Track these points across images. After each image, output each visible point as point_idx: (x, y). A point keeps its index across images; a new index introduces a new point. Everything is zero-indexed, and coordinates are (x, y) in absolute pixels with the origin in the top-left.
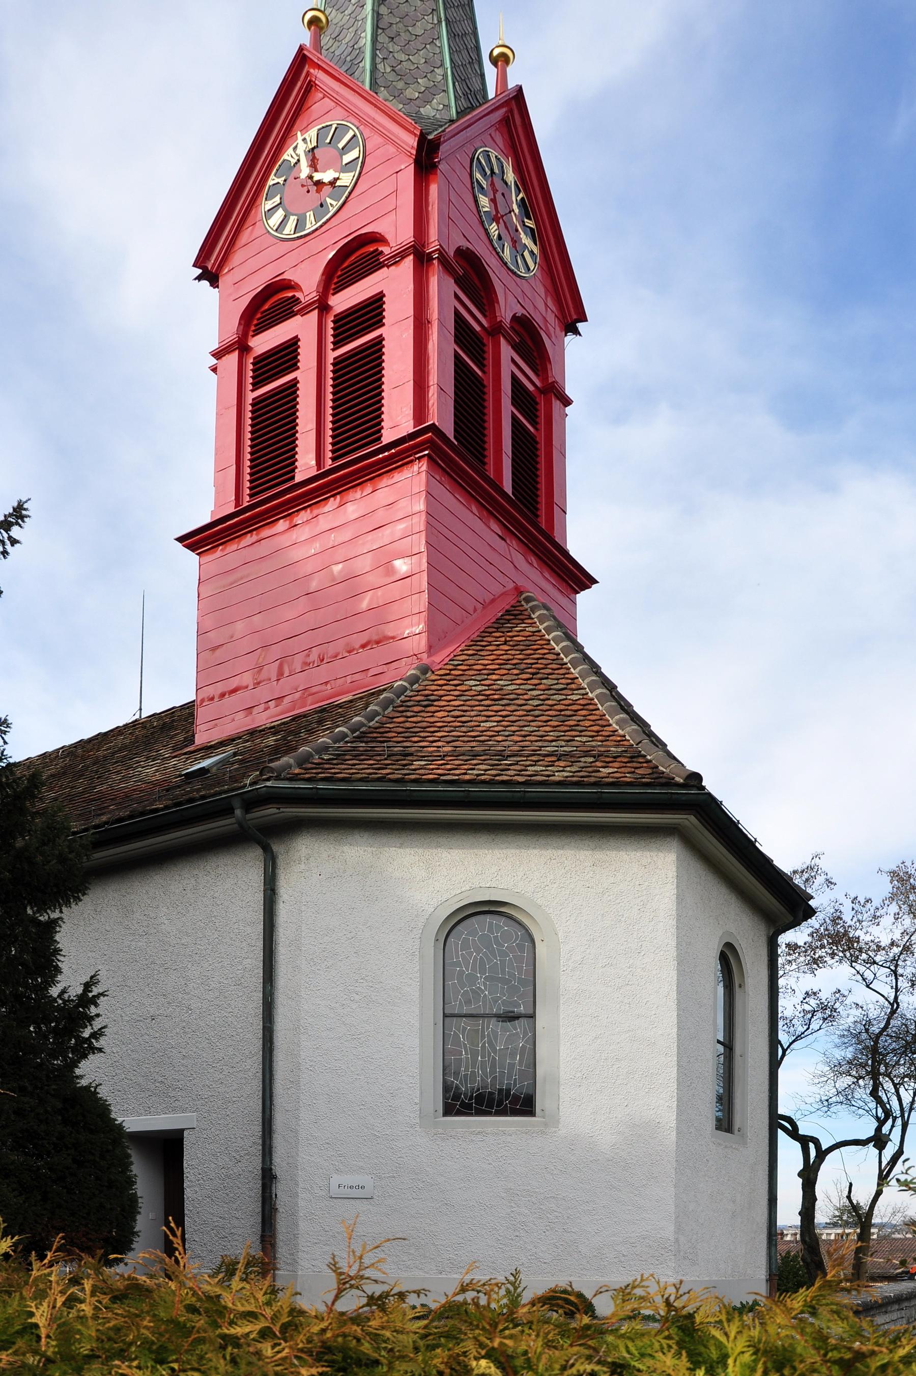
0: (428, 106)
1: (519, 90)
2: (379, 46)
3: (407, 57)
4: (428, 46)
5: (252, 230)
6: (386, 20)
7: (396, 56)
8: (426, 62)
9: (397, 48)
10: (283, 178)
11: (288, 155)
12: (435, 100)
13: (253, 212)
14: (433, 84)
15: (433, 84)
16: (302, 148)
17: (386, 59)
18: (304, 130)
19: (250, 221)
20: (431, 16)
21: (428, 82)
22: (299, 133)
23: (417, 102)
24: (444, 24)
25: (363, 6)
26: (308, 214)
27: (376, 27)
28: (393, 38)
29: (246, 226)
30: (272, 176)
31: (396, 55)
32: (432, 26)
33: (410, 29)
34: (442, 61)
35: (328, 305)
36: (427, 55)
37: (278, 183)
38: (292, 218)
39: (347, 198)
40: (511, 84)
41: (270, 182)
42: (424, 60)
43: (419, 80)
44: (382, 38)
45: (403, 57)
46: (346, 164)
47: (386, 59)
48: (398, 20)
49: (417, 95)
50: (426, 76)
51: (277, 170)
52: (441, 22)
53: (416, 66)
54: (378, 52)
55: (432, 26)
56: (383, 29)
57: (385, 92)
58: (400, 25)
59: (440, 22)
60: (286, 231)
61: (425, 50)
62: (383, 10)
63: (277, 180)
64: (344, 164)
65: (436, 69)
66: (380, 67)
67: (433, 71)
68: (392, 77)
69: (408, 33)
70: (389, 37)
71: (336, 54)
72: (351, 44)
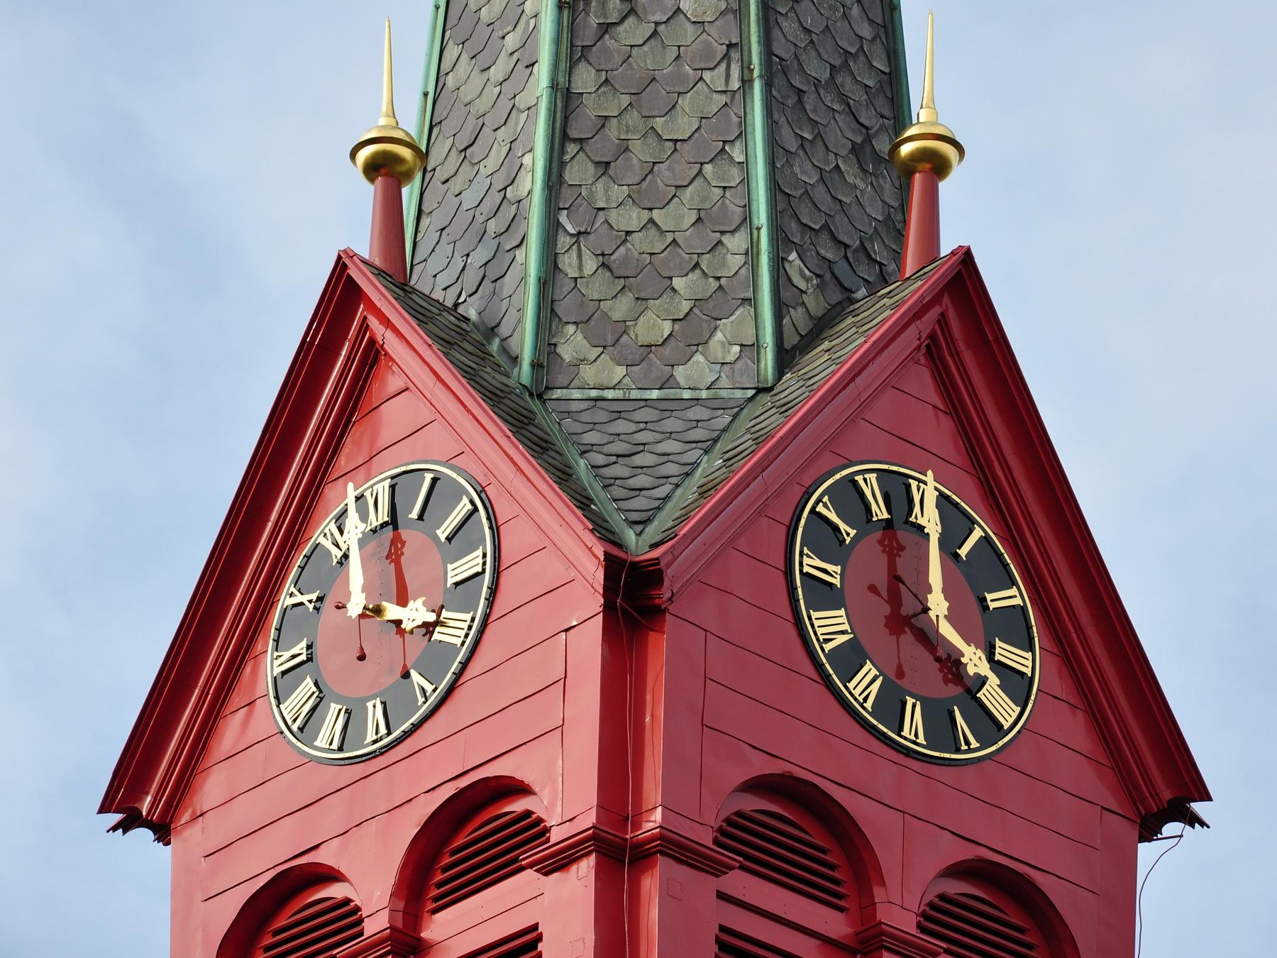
0: (699, 358)
1: (965, 258)
2: (567, 197)
3: (646, 215)
4: (708, 168)
5: (248, 717)
6: (591, 109)
7: (613, 221)
8: (699, 220)
9: (619, 192)
10: (304, 644)
11: (323, 534)
12: (719, 336)
13: (248, 670)
14: (714, 284)
15: (714, 284)
16: (355, 527)
17: (586, 233)
18: (365, 467)
19: (237, 699)
20: (723, 66)
21: (701, 282)
22: (351, 486)
23: (667, 351)
24: (757, 86)
25: (533, 65)
26: (370, 705)
27: (560, 139)
28: (608, 163)
29: (232, 706)
30: (289, 586)
31: (613, 217)
32: (724, 99)
33: (659, 123)
34: (747, 208)
35: (420, 939)
36: (703, 200)
37: (302, 604)
38: (334, 708)
39: (459, 675)
40: (946, 249)
41: (285, 600)
42: (693, 217)
43: (678, 283)
44: (579, 171)
45: (632, 218)
46: (457, 584)
47: (586, 233)
48: (625, 100)
49: (667, 327)
50: (697, 265)
51: (302, 568)
52: (751, 81)
53: (670, 238)
54: (563, 218)
55: (724, 99)
56: (581, 140)
57: (580, 337)
58: (633, 118)
59: (746, 82)
60: (321, 741)
61: (700, 180)
62: (585, 79)
63: (299, 598)
64: (450, 581)
65: (726, 239)
66: (568, 263)
67: (720, 242)
68: (597, 287)
69: (652, 140)
70: (597, 163)
71: (465, 206)
72: (499, 182)
